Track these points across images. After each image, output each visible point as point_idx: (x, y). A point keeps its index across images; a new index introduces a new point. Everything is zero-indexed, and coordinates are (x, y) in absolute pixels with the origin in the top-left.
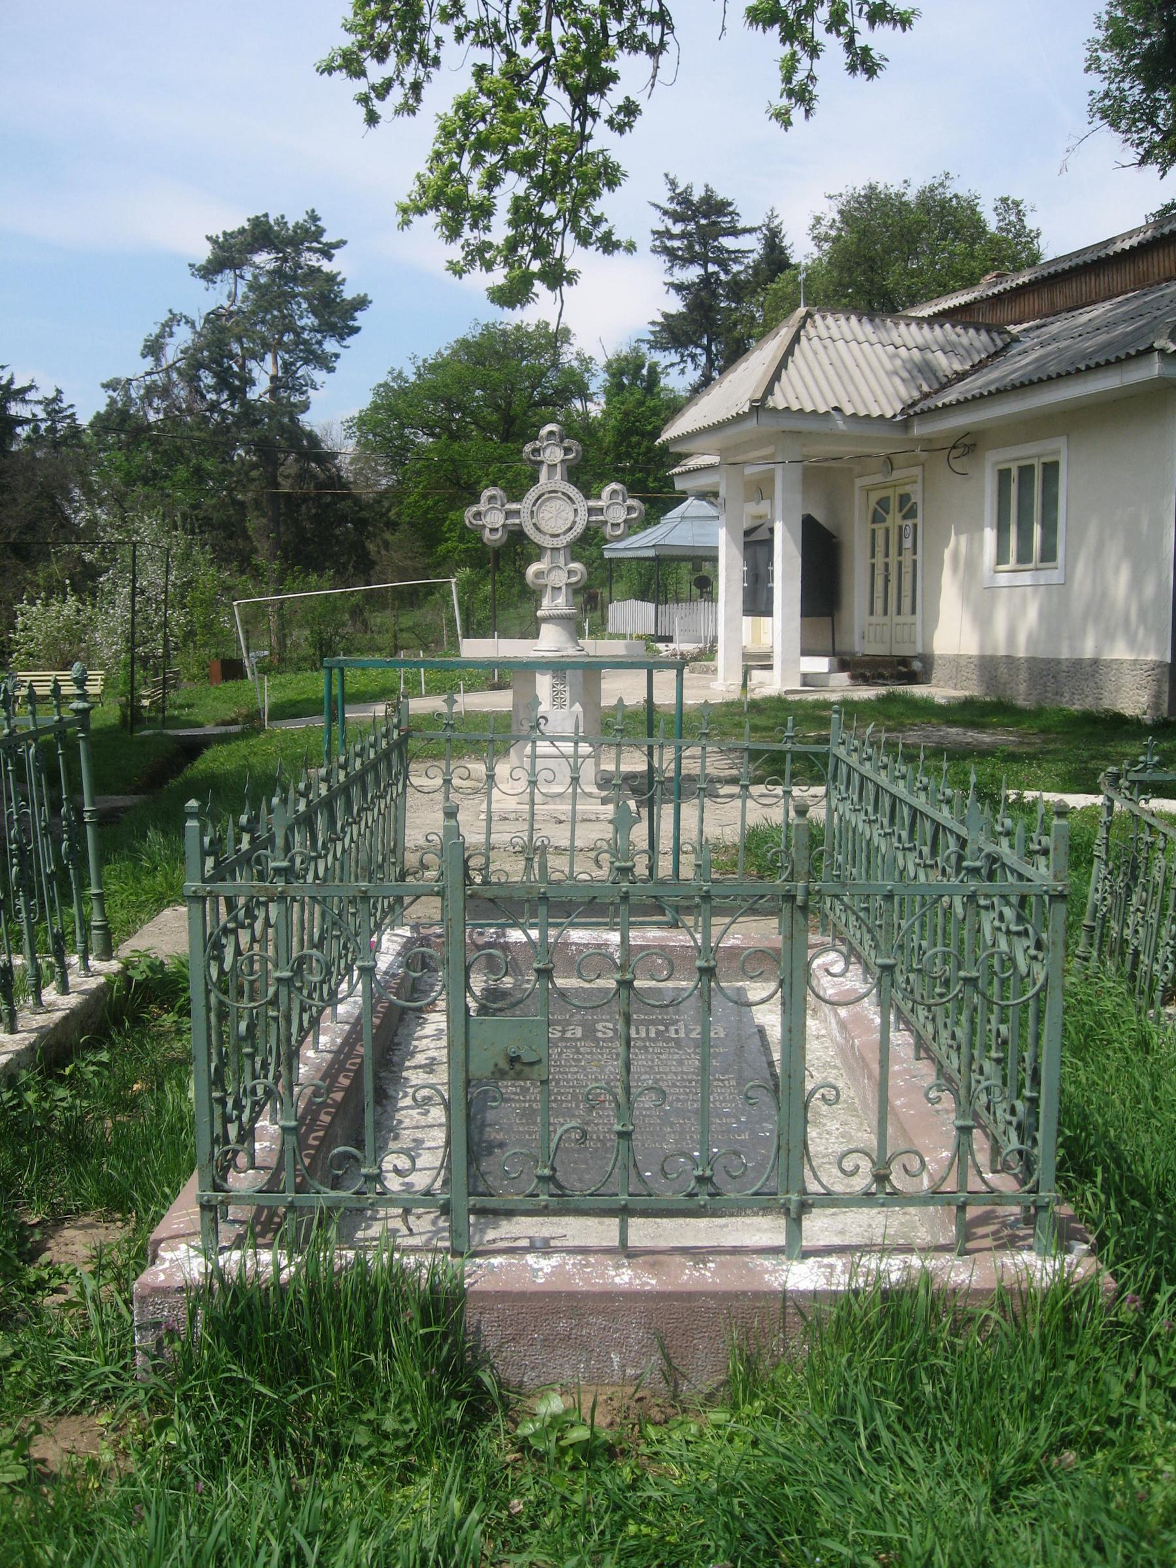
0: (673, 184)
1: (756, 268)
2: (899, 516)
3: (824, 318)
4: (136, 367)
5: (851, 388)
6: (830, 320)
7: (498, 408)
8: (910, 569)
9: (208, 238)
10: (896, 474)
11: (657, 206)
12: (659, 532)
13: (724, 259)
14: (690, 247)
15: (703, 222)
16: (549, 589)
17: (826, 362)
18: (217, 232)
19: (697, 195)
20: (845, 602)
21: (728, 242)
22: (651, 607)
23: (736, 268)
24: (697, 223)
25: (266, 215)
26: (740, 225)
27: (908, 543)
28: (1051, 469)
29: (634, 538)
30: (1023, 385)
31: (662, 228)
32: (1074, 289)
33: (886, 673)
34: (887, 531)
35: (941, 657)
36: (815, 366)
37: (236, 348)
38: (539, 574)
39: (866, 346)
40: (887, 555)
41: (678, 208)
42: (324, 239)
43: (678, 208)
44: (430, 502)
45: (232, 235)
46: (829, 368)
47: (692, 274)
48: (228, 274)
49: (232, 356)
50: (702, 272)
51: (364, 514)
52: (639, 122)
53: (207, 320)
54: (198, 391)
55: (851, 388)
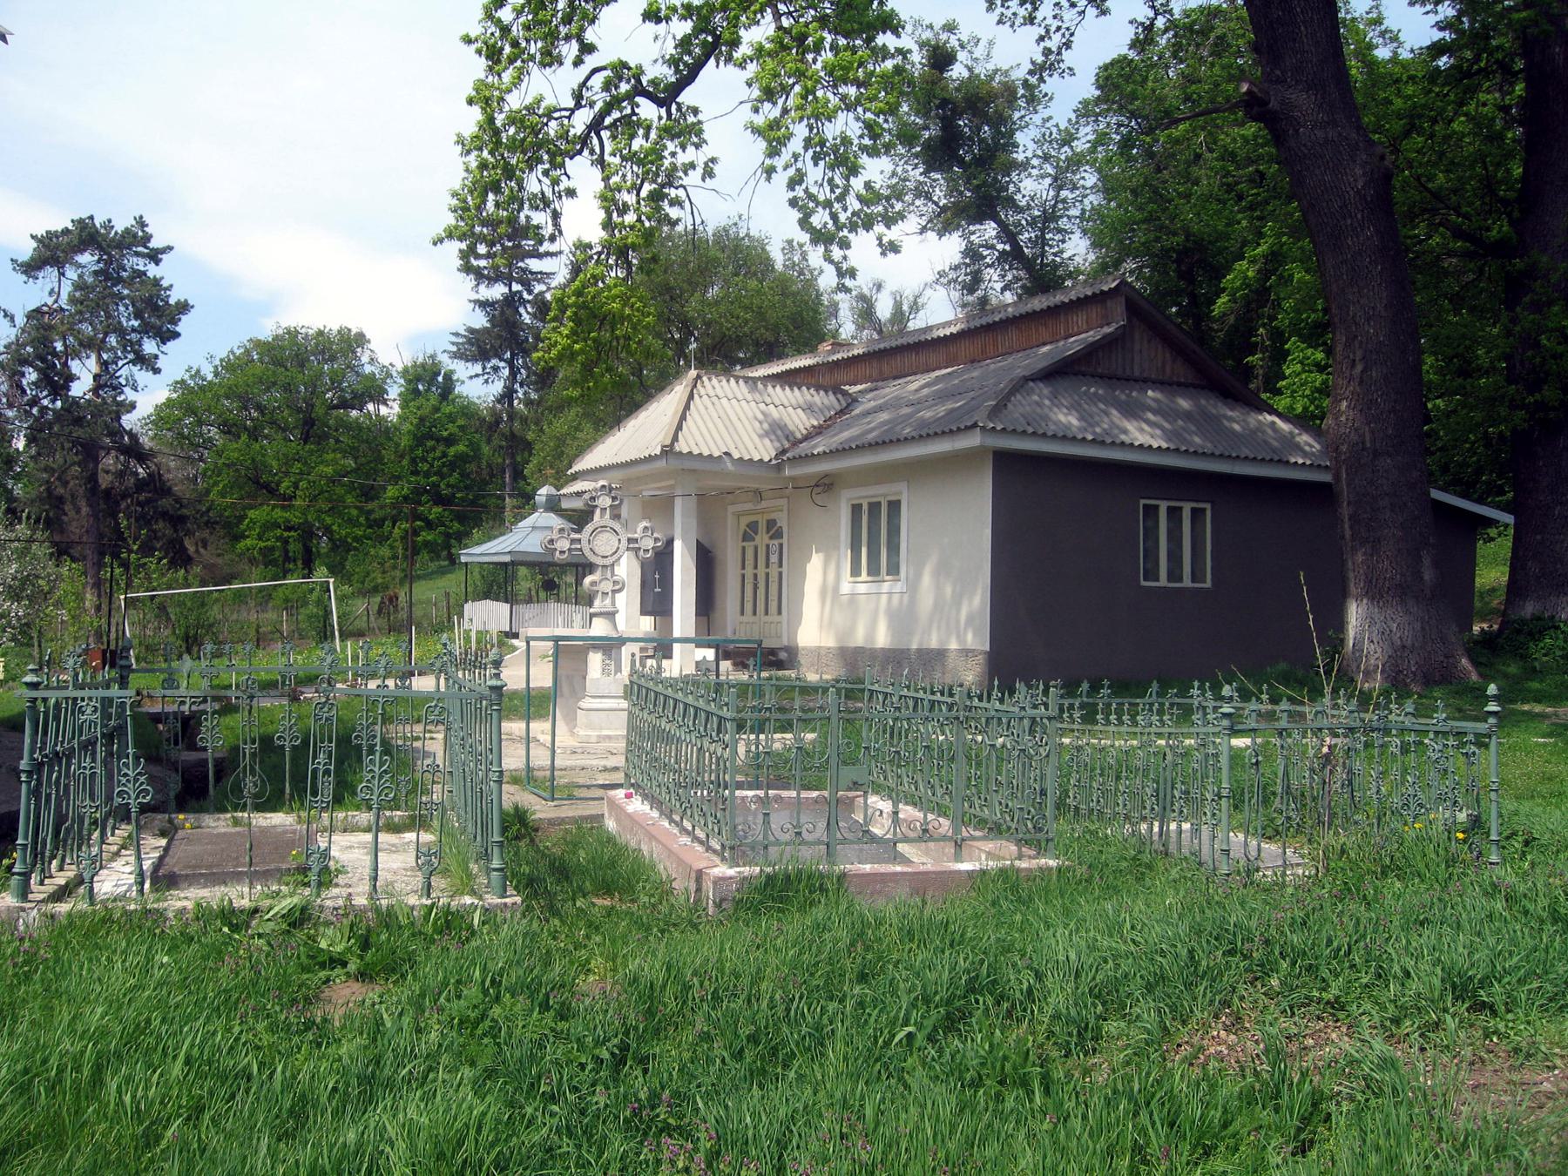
2: (766, 537)
3: (710, 379)
5: (736, 437)
6: (714, 380)
7: (299, 410)
8: (776, 579)
9: (32, 237)
10: (764, 504)
12: (511, 540)
13: (527, 279)
14: (495, 268)
17: (715, 415)
18: (41, 232)
20: (718, 602)
21: (534, 264)
25: (91, 218)
27: (774, 558)
28: (895, 506)
29: (489, 545)
30: (877, 443)
32: (897, 362)
34: (756, 548)
35: (804, 649)
36: (706, 417)
37: (59, 346)
38: (593, 583)
39: (743, 403)
40: (756, 567)
42: (151, 245)
46: (718, 421)
47: (497, 291)
48: (51, 273)
49: (55, 354)
50: (506, 290)
51: (185, 511)
53: (31, 316)
54: (20, 387)
55: (736, 437)
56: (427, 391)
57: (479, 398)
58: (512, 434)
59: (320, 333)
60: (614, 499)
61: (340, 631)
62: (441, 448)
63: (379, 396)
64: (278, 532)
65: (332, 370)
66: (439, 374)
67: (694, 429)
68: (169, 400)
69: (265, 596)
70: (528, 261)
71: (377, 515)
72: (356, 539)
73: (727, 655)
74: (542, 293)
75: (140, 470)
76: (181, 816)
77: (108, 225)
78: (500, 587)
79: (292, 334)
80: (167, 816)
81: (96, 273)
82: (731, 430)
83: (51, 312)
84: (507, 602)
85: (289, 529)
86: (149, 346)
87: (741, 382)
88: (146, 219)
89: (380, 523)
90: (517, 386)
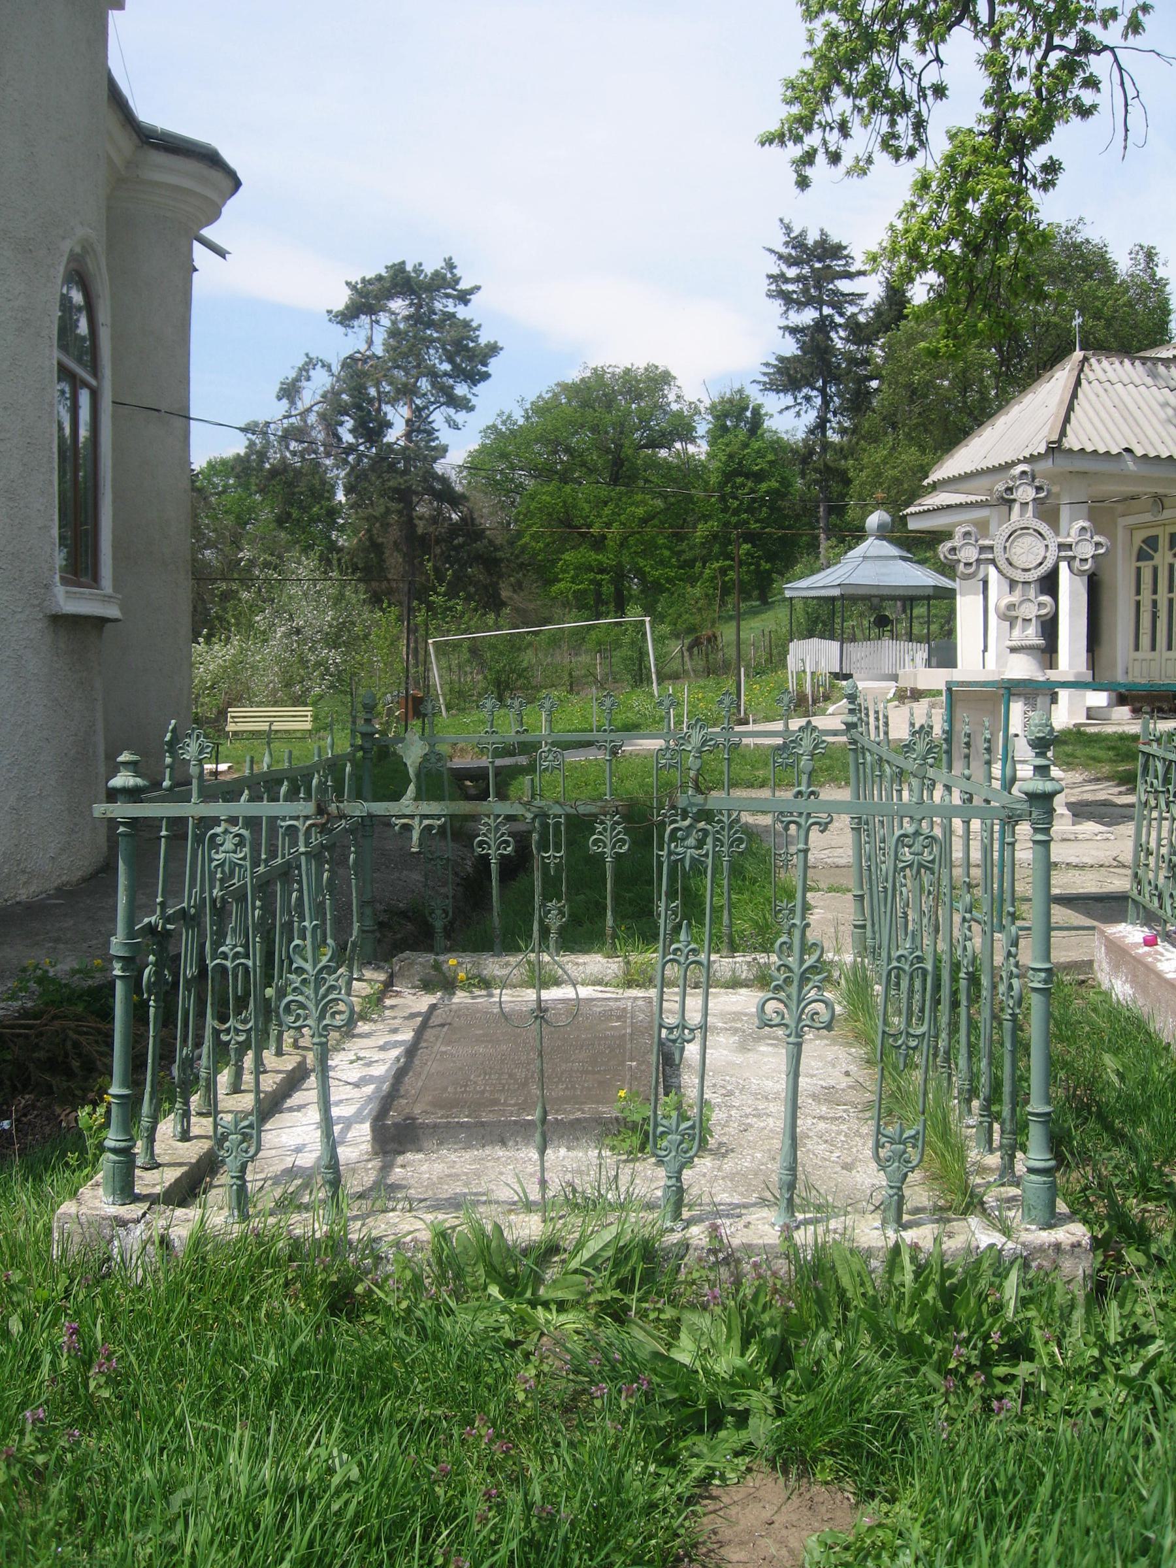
0: (788, 229)
1: (878, 310)
3: (1099, 361)
4: (273, 411)
5: (1137, 430)
6: (1105, 363)
7: (608, 451)
9: (348, 284)
11: (772, 251)
13: (839, 301)
14: (805, 291)
15: (818, 265)
16: (1020, 621)
17: (1109, 404)
18: (355, 278)
19: (812, 238)
21: (844, 286)
22: (835, 646)
23: (850, 310)
24: (811, 267)
26: (853, 269)
31: (776, 271)
33: (1165, 707)
34: (1155, 570)
36: (1099, 407)
37: (373, 392)
40: (1155, 592)
41: (793, 253)
43: (793, 253)
44: (541, 545)
45: (370, 282)
47: (808, 316)
48: (364, 319)
49: (370, 401)
51: (499, 554)
52: (1062, 179)
53: (344, 365)
56: (736, 427)
57: (787, 432)
58: (826, 465)
59: (627, 371)
60: (1039, 489)
61: (658, 673)
62: (750, 484)
63: (687, 434)
64: (591, 576)
65: (640, 409)
66: (746, 409)
67: (1084, 420)
68: (484, 445)
69: (579, 636)
70: (838, 282)
71: (687, 556)
72: (668, 580)
73: (1122, 700)
74: (854, 315)
75: (454, 516)
76: (452, 962)
77: (418, 269)
78: (825, 625)
79: (598, 374)
80: (431, 957)
81: (407, 318)
82: (1130, 420)
83: (365, 360)
84: (832, 638)
85: (602, 571)
86: (461, 390)
87: (1137, 363)
88: (455, 261)
89: (690, 564)
90: (830, 416)
